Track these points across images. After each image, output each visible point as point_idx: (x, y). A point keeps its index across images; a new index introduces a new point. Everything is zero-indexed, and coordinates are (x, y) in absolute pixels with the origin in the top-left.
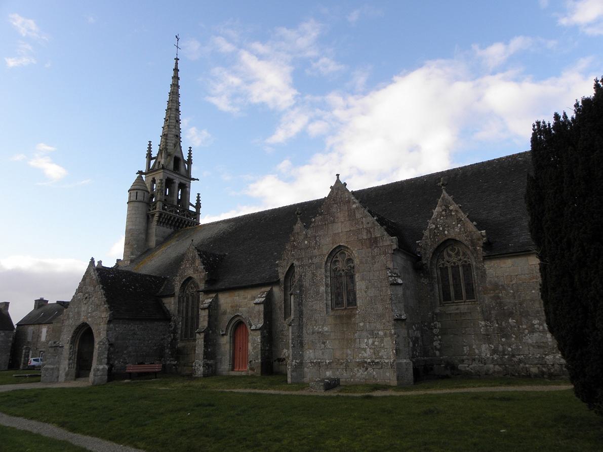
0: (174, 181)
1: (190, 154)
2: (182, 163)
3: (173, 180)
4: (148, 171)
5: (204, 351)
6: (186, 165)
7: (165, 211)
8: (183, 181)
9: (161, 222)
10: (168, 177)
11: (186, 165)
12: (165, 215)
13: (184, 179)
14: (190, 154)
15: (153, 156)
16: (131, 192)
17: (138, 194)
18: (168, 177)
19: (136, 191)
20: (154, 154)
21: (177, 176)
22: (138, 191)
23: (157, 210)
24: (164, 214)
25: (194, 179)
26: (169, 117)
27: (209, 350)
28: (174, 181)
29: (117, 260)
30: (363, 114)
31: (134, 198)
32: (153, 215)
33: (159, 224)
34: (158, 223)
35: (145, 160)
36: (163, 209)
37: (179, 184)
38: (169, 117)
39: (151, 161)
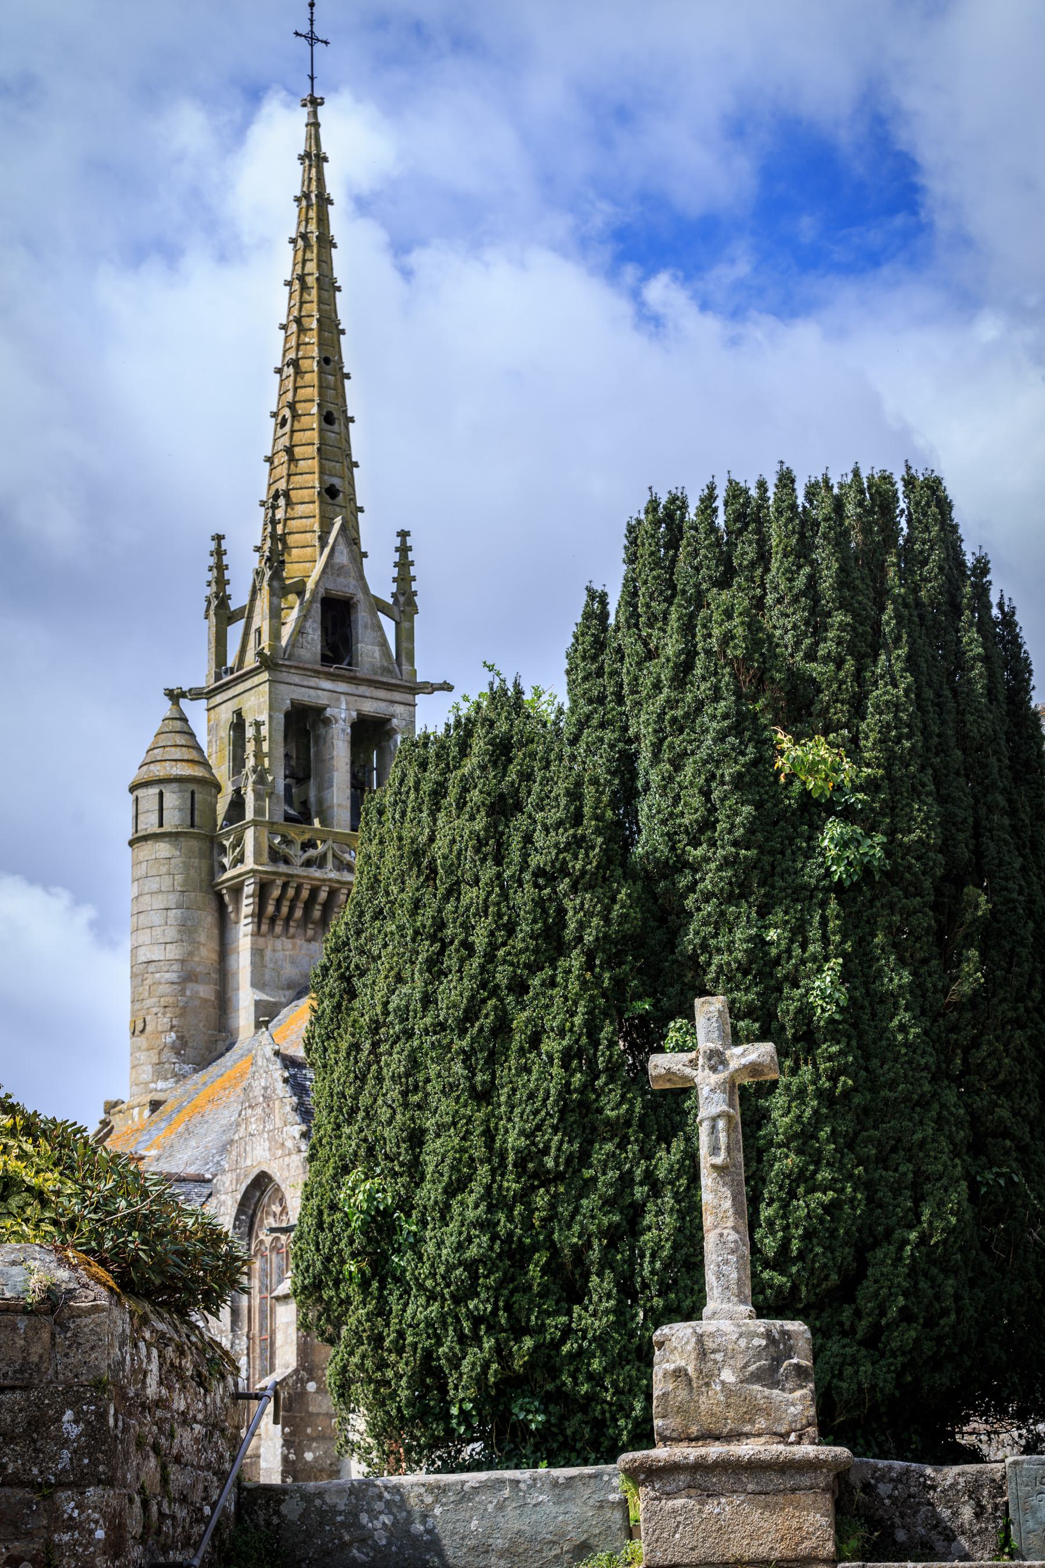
0: (329, 712)
1: (404, 564)
2: (362, 615)
3: (319, 710)
4: (218, 677)
5: (285, 1459)
6: (388, 626)
7: (282, 868)
8: (369, 707)
9: (273, 920)
10: (293, 702)
11: (388, 626)
12: (285, 886)
13: (381, 694)
14: (404, 564)
15: (234, 605)
16: (140, 793)
17: (156, 821)
18: (293, 702)
19: (154, 791)
20: (238, 599)
21: (342, 687)
22: (162, 787)
23: (249, 863)
24: (279, 882)
25: (430, 688)
26: (292, 406)
27: (309, 1456)
28: (329, 712)
29: (107, 1103)
30: (518, 704)
31: (149, 823)
32: (237, 891)
33: (264, 928)
34: (259, 924)
35: (205, 630)
36: (275, 856)
37: (354, 726)
38: (292, 406)
39: (230, 629)
